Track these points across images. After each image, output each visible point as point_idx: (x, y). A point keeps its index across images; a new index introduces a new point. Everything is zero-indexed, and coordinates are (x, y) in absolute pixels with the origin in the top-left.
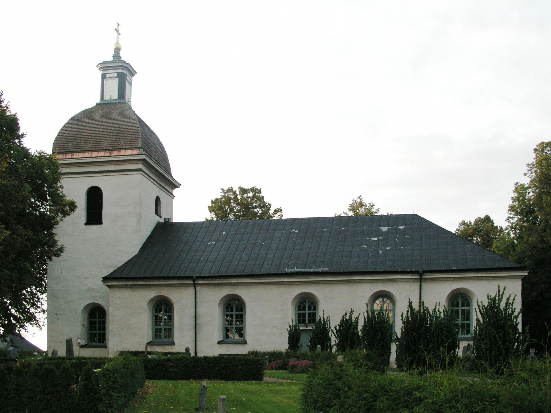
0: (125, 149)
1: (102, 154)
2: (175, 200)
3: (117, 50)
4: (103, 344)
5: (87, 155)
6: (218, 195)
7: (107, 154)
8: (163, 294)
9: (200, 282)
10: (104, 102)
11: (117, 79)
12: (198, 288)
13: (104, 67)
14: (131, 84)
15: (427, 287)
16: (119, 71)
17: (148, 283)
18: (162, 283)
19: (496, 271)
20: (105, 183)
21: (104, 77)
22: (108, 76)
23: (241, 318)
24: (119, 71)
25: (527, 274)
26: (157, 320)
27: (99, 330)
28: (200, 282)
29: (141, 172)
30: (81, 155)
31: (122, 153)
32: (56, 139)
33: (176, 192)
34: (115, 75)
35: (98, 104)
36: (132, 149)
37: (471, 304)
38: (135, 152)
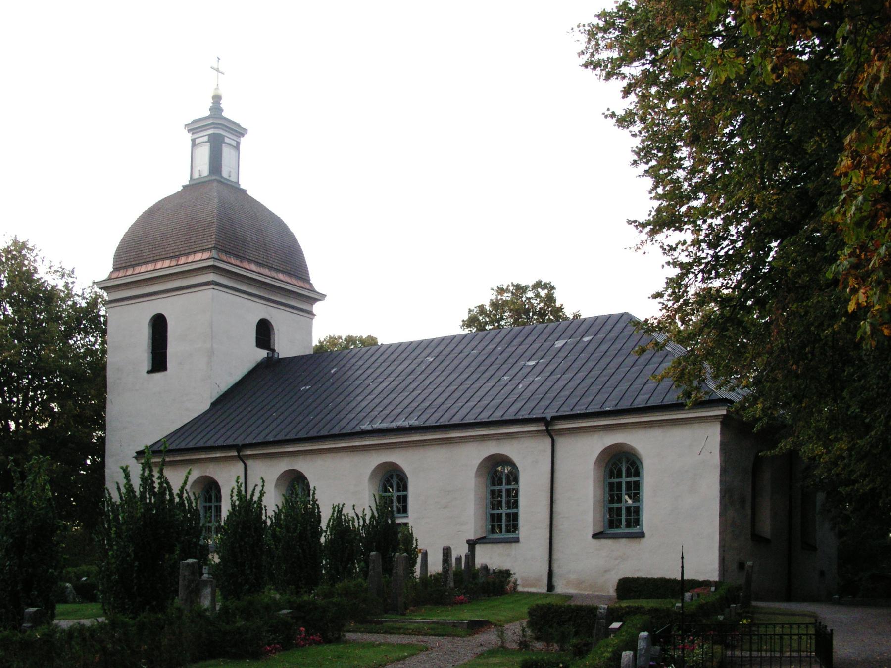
0: (195, 252)
1: (167, 263)
2: (315, 321)
3: (217, 99)
4: (511, 536)
5: (151, 267)
6: (486, 298)
7: (174, 263)
8: (296, 467)
9: (249, 452)
10: (193, 182)
11: (208, 144)
12: (249, 463)
13: (194, 127)
14: (237, 147)
15: (563, 444)
16: (218, 133)
17: (187, 458)
18: (203, 456)
19: (642, 413)
20: (173, 308)
21: (194, 144)
22: (198, 141)
23: (635, 490)
24: (218, 133)
25: (724, 412)
26: (495, 500)
27: (500, 515)
28: (249, 452)
29: (212, 286)
30: (143, 268)
31: (191, 258)
32: (119, 249)
33: (317, 308)
34: (206, 139)
35: (185, 187)
36: (203, 251)
37: (641, 471)
38: (206, 255)
